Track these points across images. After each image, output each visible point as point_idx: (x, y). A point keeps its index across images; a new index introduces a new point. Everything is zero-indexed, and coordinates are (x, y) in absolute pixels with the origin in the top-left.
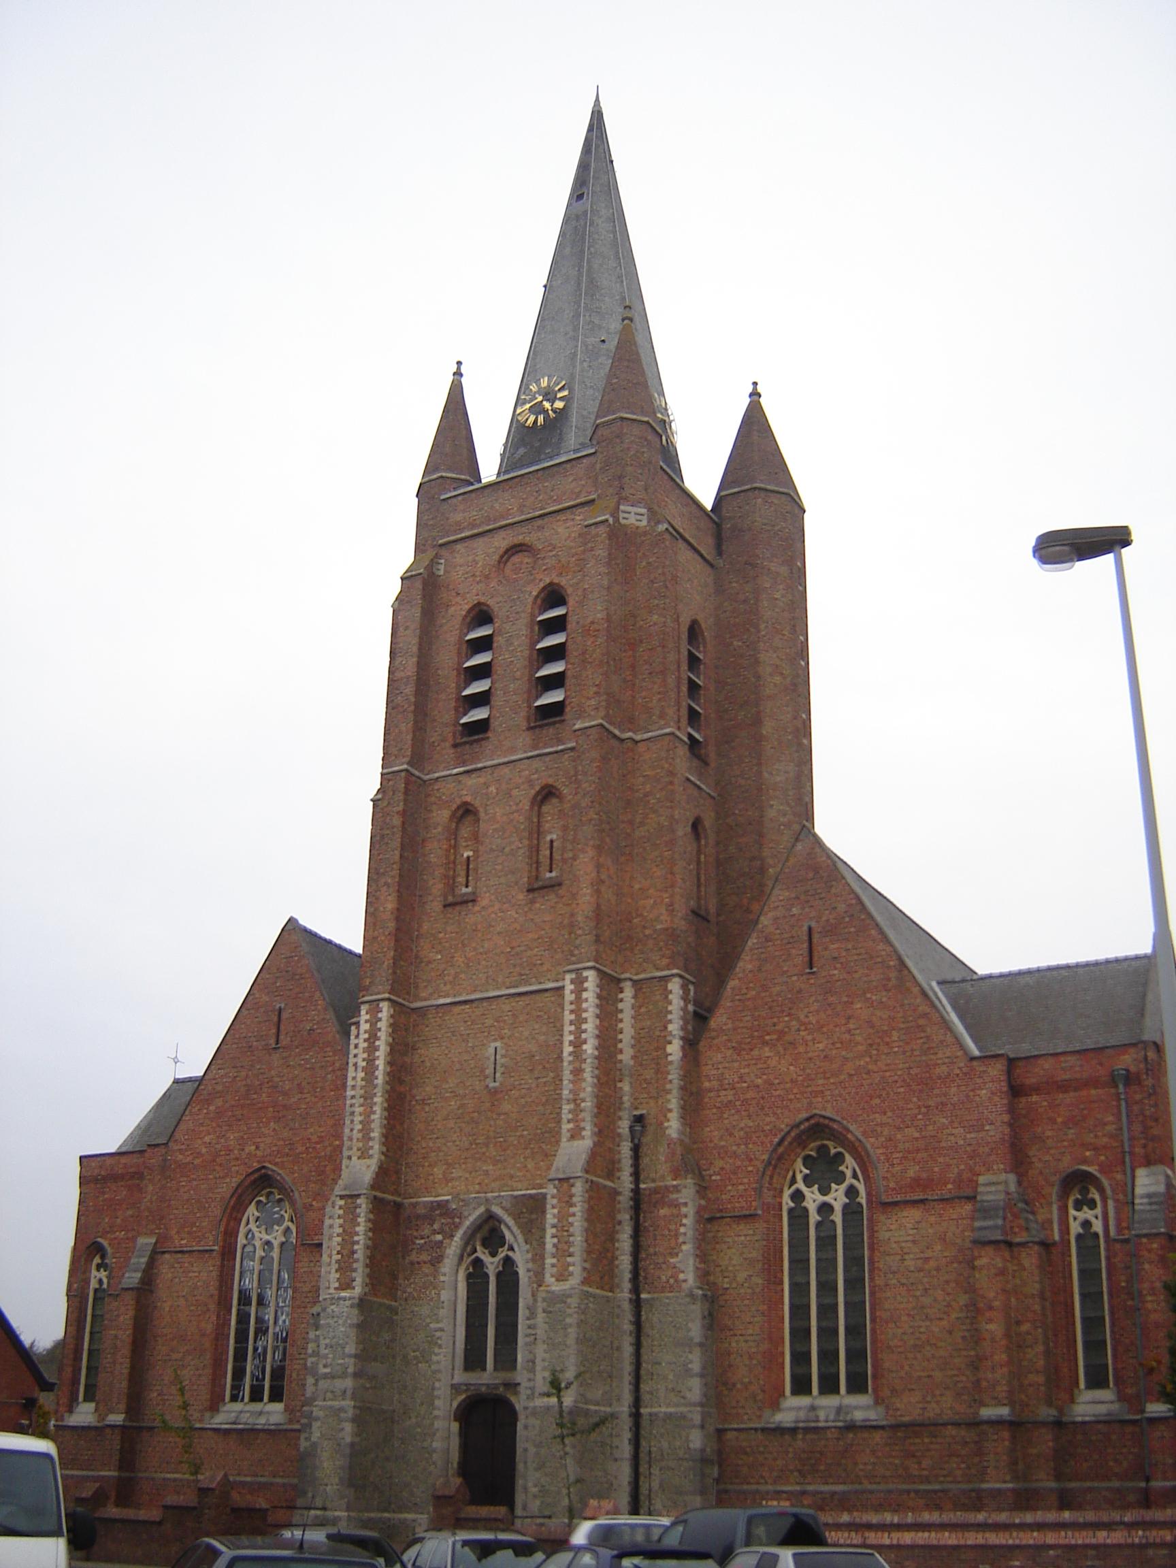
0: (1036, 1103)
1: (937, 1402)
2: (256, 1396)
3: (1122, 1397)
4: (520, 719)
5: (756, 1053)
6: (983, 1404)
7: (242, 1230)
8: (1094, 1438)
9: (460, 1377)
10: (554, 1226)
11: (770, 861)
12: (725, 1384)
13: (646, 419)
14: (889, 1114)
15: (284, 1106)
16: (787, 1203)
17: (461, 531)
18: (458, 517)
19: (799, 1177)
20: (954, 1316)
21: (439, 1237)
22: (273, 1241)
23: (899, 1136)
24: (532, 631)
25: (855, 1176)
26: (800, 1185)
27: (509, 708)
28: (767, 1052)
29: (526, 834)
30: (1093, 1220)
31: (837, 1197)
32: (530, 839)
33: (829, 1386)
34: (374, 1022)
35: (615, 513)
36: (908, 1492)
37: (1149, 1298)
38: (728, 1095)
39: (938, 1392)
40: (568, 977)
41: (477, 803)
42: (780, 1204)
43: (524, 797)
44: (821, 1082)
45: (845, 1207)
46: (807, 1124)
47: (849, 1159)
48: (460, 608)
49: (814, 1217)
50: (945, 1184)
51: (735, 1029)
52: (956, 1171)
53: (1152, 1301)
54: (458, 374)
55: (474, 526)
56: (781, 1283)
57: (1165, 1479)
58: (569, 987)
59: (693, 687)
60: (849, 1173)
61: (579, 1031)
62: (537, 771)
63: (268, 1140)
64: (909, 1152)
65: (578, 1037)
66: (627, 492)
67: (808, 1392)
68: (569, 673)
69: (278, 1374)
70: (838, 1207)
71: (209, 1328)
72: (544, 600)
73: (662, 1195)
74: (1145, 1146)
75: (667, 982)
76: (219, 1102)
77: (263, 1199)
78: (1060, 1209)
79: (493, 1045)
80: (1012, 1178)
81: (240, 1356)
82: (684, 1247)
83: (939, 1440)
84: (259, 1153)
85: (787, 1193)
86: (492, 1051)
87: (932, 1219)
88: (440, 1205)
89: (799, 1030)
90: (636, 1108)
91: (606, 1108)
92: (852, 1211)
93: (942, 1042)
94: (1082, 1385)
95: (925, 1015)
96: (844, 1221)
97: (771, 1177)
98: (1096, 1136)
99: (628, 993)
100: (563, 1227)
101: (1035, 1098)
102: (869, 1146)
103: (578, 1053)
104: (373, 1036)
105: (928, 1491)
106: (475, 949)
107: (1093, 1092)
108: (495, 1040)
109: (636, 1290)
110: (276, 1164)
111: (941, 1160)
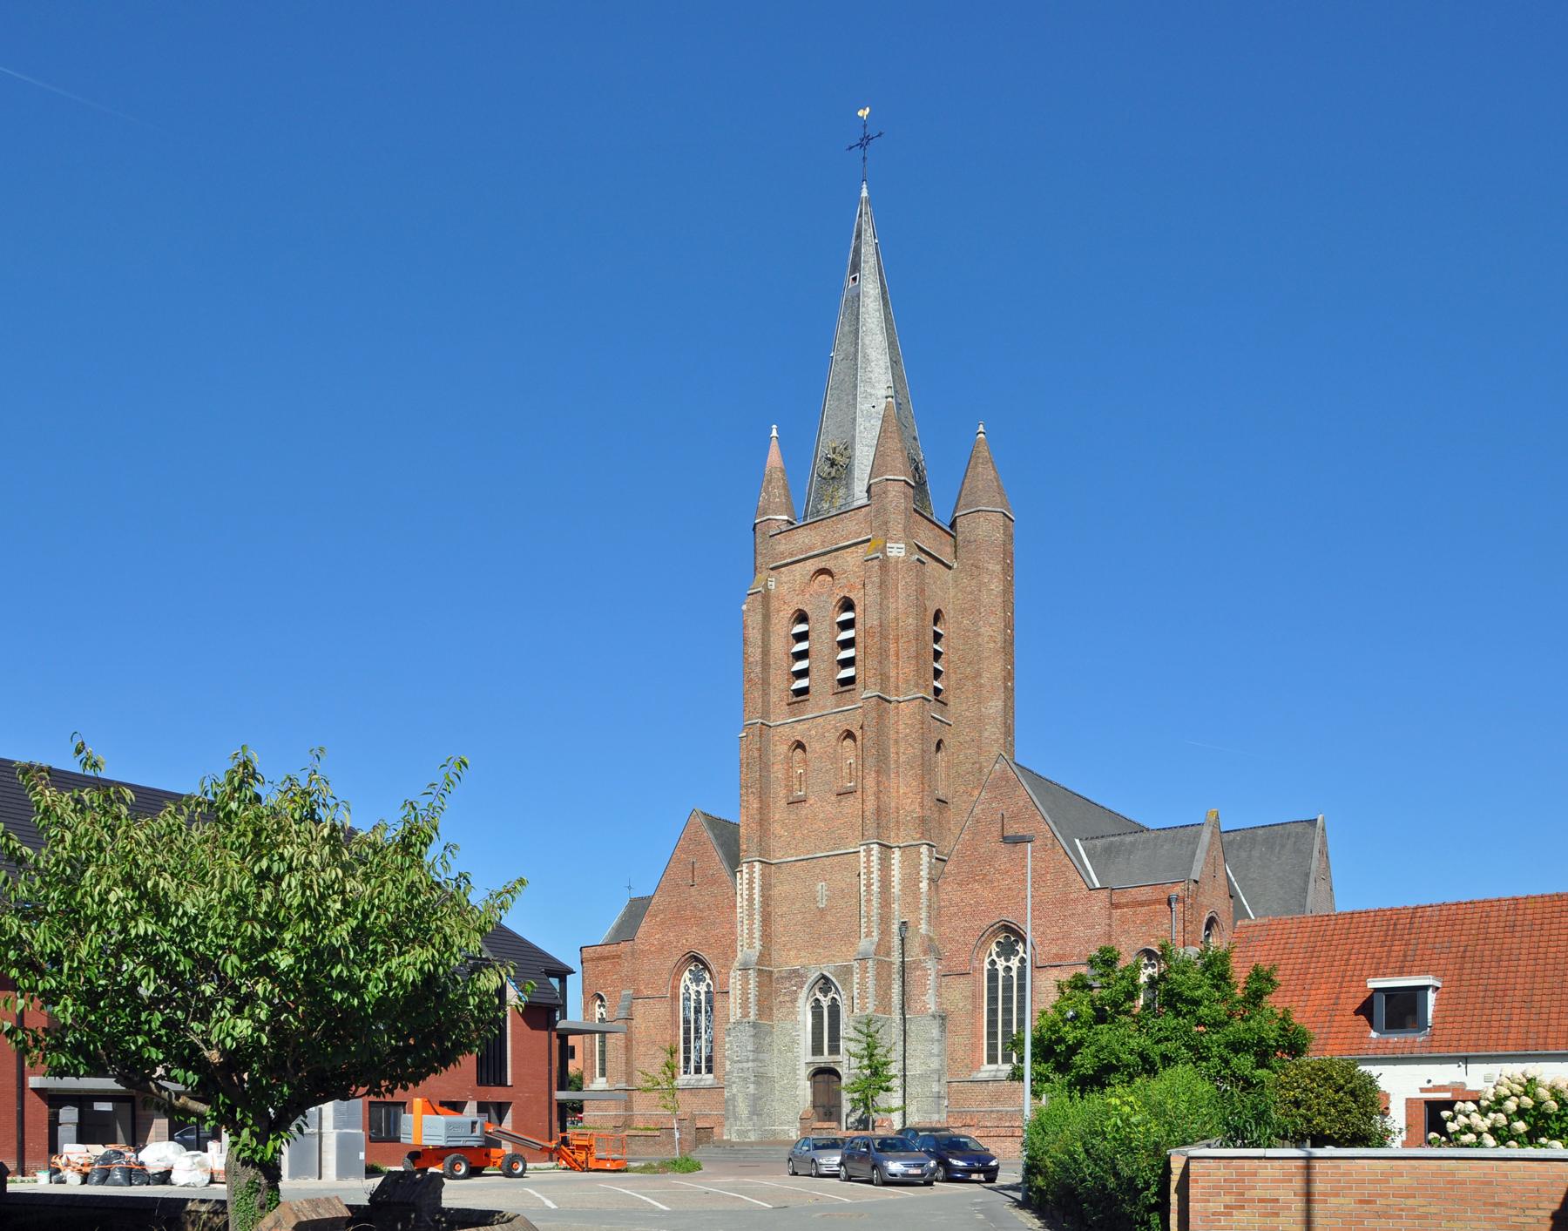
2: (698, 1070)
4: (830, 686)
9: (810, 1058)
16: (987, 966)
18: (782, 548)
26: (994, 957)
27: (822, 679)
28: (976, 886)
34: (751, 873)
38: (954, 909)
48: (788, 612)
49: (1001, 973)
55: (791, 555)
58: (862, 854)
59: (937, 637)
61: (869, 879)
66: (892, 533)
69: (709, 1059)
81: (687, 1051)
88: (795, 971)
91: (885, 920)
99: (897, 854)
100: (862, 985)
103: (868, 890)
104: (751, 882)
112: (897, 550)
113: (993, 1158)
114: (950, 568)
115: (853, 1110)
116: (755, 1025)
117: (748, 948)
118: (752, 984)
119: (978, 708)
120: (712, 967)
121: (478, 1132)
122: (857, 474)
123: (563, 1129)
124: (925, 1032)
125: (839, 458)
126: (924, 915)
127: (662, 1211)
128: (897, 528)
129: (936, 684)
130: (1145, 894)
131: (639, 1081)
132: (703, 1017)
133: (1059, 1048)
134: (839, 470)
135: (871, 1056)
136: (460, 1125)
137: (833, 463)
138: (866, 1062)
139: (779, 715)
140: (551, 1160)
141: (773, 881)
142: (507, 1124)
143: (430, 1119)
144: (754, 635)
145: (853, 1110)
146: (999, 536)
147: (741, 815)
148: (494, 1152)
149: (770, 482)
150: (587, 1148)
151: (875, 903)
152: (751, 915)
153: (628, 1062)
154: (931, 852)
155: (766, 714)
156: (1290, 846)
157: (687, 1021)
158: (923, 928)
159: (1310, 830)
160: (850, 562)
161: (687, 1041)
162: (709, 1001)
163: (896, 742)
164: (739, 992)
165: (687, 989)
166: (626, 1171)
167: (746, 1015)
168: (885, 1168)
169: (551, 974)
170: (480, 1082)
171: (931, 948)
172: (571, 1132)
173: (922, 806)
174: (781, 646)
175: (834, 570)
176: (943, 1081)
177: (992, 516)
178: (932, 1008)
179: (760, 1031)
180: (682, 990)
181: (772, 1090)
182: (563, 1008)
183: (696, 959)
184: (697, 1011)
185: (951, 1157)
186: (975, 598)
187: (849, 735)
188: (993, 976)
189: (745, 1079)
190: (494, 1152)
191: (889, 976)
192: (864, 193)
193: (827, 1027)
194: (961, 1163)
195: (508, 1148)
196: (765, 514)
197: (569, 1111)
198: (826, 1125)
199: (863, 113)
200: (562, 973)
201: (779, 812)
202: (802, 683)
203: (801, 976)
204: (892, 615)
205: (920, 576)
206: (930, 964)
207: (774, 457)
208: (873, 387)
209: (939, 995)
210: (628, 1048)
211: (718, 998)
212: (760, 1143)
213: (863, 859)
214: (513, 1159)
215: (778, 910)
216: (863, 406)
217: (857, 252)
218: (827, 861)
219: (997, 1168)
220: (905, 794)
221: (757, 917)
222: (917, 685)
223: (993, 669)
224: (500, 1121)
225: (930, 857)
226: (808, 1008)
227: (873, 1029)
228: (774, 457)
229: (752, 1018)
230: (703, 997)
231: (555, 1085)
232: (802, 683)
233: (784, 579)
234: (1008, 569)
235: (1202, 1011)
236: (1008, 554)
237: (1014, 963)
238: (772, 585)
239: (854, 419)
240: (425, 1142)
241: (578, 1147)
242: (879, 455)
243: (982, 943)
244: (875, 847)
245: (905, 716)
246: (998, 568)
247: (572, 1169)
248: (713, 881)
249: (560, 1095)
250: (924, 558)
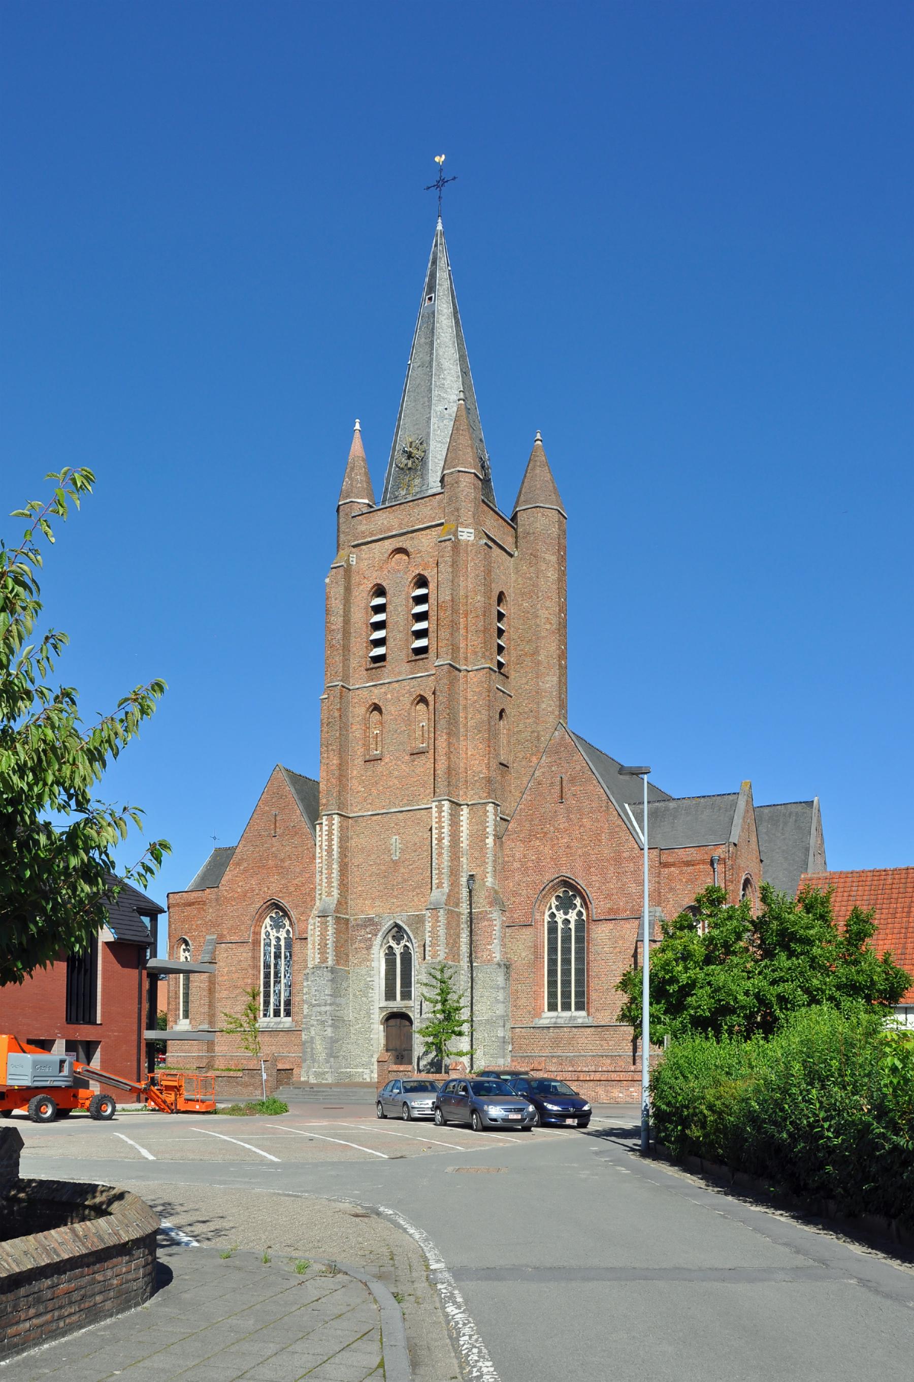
7: (263, 931)
9: (383, 1004)
11: (542, 733)
13: (473, 471)
16: (547, 918)
17: (365, 537)
18: (363, 528)
21: (370, 936)
27: (398, 646)
28: (538, 843)
33: (566, 1007)
34: (330, 825)
35: (455, 534)
40: (434, 804)
41: (380, 704)
48: (369, 585)
49: (560, 926)
55: (372, 534)
58: (434, 810)
59: (500, 616)
63: (274, 885)
67: (556, 1010)
68: (430, 630)
69: (288, 1003)
73: (484, 915)
81: (267, 995)
88: (371, 919)
91: (454, 872)
92: (580, 925)
95: (619, 826)
99: (465, 811)
100: (435, 935)
101: (672, 869)
104: (330, 833)
107: (701, 866)
109: (471, 962)
112: (467, 535)
113: (586, 1103)
114: (511, 556)
115: (426, 1053)
116: (333, 971)
117: (326, 896)
118: (331, 931)
119: (537, 682)
120: (292, 913)
121: (66, 1072)
122: (430, 465)
123: (151, 1069)
124: (491, 981)
125: (415, 452)
126: (490, 869)
127: (272, 1164)
128: (467, 513)
129: (499, 658)
130: (693, 854)
131: (222, 1023)
132: (282, 962)
133: (672, 989)
134: (415, 462)
135: (444, 1002)
136: (45, 1065)
137: (410, 456)
138: (439, 1006)
139: (359, 680)
140: (139, 1101)
141: (350, 834)
142: (96, 1063)
143: (17, 1057)
144: (337, 605)
145: (426, 1053)
146: (554, 530)
147: (321, 774)
148: (82, 1093)
149: (352, 469)
150: (177, 1089)
151: (445, 852)
152: (329, 867)
153: (211, 1005)
154: (496, 811)
155: (346, 678)
156: (791, 822)
157: (267, 966)
158: (490, 881)
159: (807, 810)
160: (425, 543)
161: (267, 985)
162: (289, 945)
163: (465, 708)
164: (317, 936)
165: (268, 934)
166: (215, 1112)
167: (324, 960)
168: (486, 1113)
169: (143, 912)
170: (70, 1020)
171: (496, 900)
172: (158, 1073)
173: (488, 768)
174: (360, 617)
175: (410, 550)
176: (508, 1026)
177: (548, 512)
178: (497, 957)
179: (337, 976)
180: (263, 936)
181: (348, 1033)
182: (153, 945)
183: (277, 906)
184: (277, 956)
185: (549, 1104)
186: (535, 585)
187: (422, 700)
188: (553, 929)
189: (323, 1023)
190: (82, 1093)
191: (458, 925)
192: (440, 227)
193: (400, 973)
194: (555, 1108)
195: (95, 1088)
196: (348, 496)
197: (156, 1050)
198: (402, 1068)
199: (440, 159)
200: (153, 912)
201: (356, 769)
202: (380, 651)
203: (376, 924)
204: (462, 593)
205: (487, 557)
206: (495, 915)
207: (357, 447)
208: (446, 392)
209: (504, 945)
210: (211, 991)
211: (297, 947)
212: (337, 1085)
213: (435, 815)
214: (102, 1100)
215: (356, 860)
216: (438, 408)
217: (433, 276)
218: (400, 816)
219: (589, 1113)
220: (472, 756)
221: (335, 866)
222: (484, 657)
223: (549, 648)
224: (89, 1060)
225: (496, 815)
226: (382, 955)
227: (446, 975)
228: (357, 447)
229: (330, 963)
230: (282, 943)
231: (144, 1025)
232: (380, 651)
233: (364, 556)
234: (562, 560)
235: (816, 951)
236: (561, 547)
237: (572, 916)
238: (353, 560)
239: (429, 419)
240: (10, 1083)
241: (168, 1088)
242: (451, 449)
243: (543, 895)
244: (446, 803)
245: (474, 683)
246: (553, 559)
247: (161, 1110)
248: (295, 832)
249: (149, 1035)
250: (490, 544)
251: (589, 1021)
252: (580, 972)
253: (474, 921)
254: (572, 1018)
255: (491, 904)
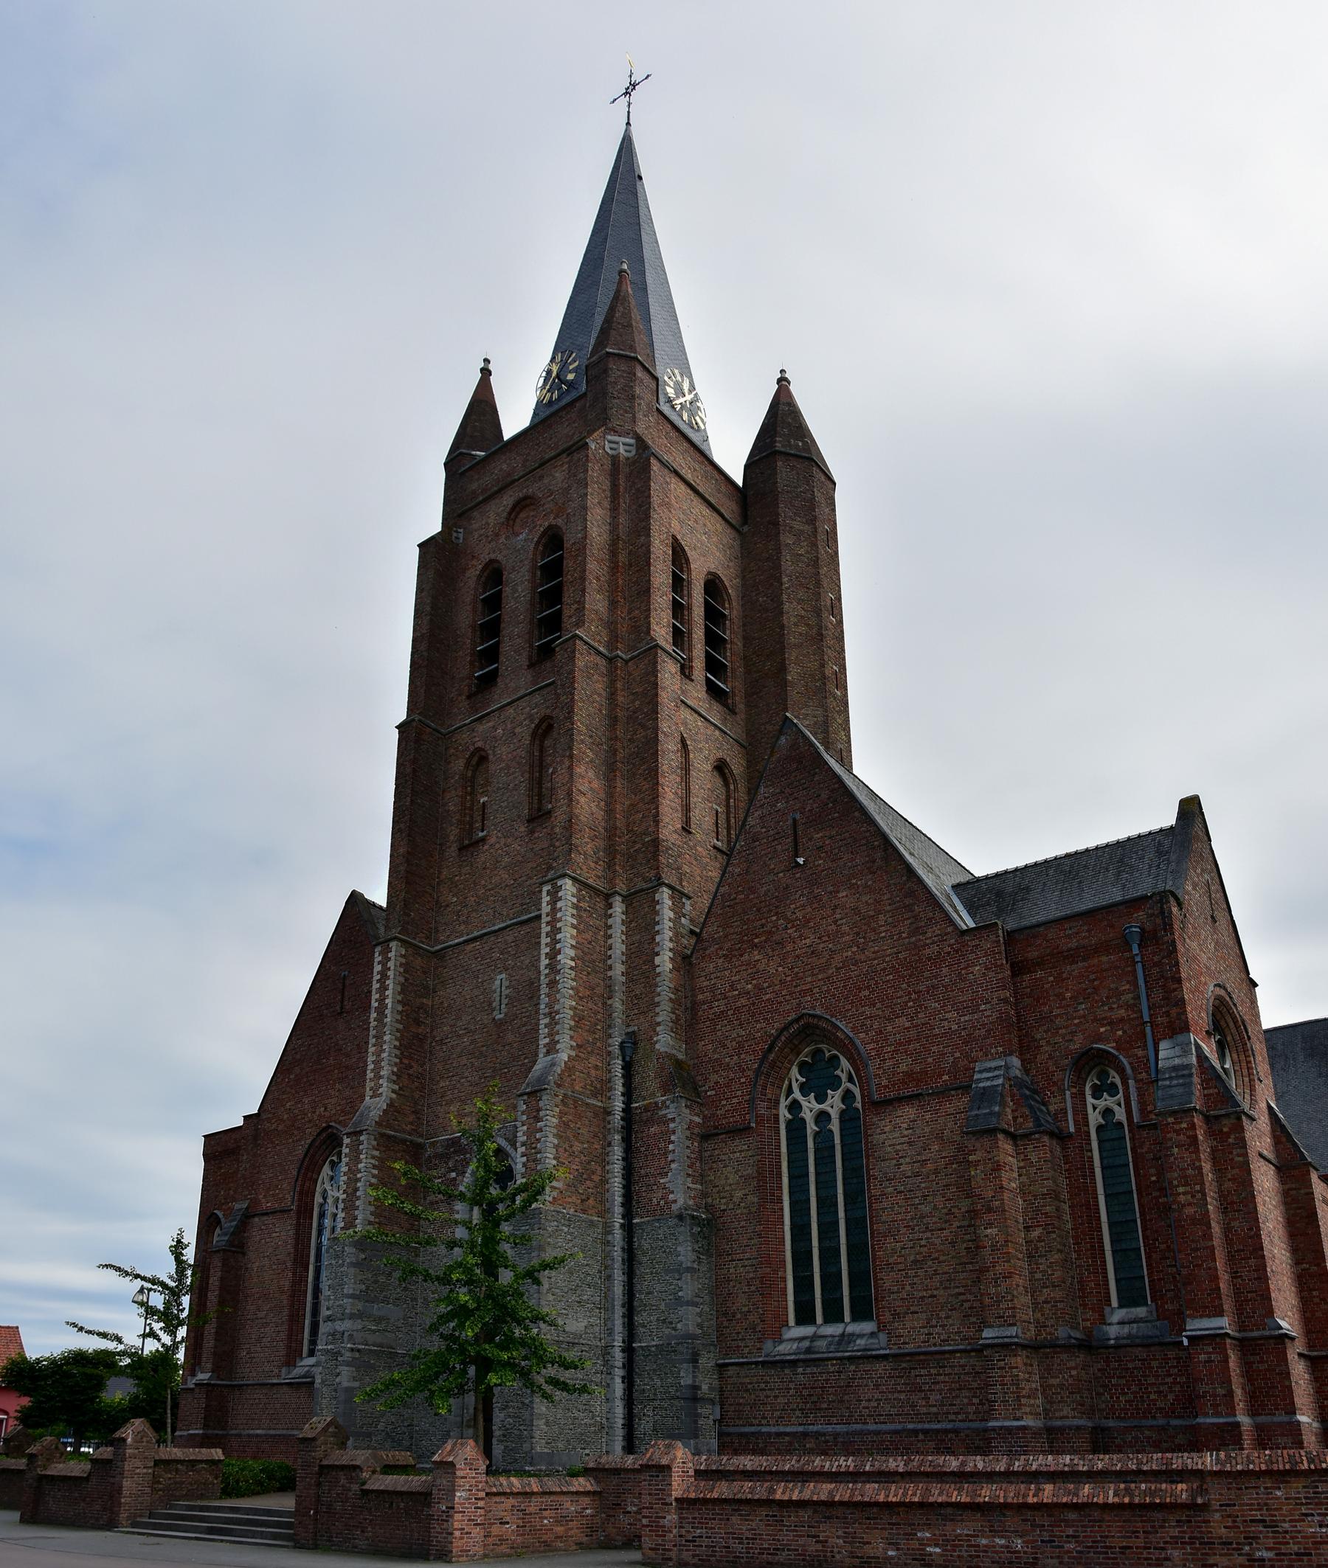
0: (1041, 979)
1: (943, 1326)
3: (1161, 1314)
5: (746, 957)
6: (985, 1324)
8: (1130, 1365)
10: (523, 1144)
12: (725, 1314)
14: (878, 1005)
15: (347, 1067)
16: (784, 1114)
18: (474, 486)
19: (795, 1086)
20: (956, 1224)
22: (829, 1110)
23: (890, 1028)
24: (534, 574)
25: (850, 1080)
26: (797, 1094)
29: (527, 768)
30: (1116, 1108)
31: (834, 1104)
32: (531, 773)
33: (833, 1315)
36: (915, 1432)
37: (1181, 1190)
38: (719, 1006)
39: (943, 1314)
42: (777, 1117)
43: (524, 731)
44: (809, 979)
45: (842, 1113)
46: (796, 1026)
47: (844, 1063)
49: (811, 1127)
50: (940, 1076)
51: (726, 936)
52: (951, 1059)
53: (1184, 1194)
54: (486, 372)
56: (780, 1201)
57: (1217, 1414)
60: (844, 1077)
62: (537, 705)
63: (333, 1101)
64: (900, 1044)
65: (553, 949)
70: (834, 1114)
71: (287, 1284)
72: (545, 546)
74: (1168, 1014)
75: (654, 893)
76: (297, 1070)
77: (335, 1158)
78: (1073, 1096)
79: (499, 977)
80: (1015, 1061)
82: (673, 1166)
83: (948, 1370)
84: (327, 1114)
85: (783, 1104)
86: (498, 982)
87: (928, 1116)
88: (455, 1142)
89: (786, 928)
90: (628, 1026)
92: (848, 1117)
93: (930, 919)
94: (1115, 1303)
96: (841, 1130)
97: (764, 1088)
98: (1111, 1009)
101: (1039, 974)
102: (858, 1042)
105: (938, 1431)
106: (484, 886)
107: (1104, 959)
108: (500, 973)
109: (628, 1215)
110: (340, 1123)
111: (934, 1049)
251: (881, 1344)
252: (856, 1225)
253: (635, 1127)
254: (845, 1339)
255: (666, 1089)
